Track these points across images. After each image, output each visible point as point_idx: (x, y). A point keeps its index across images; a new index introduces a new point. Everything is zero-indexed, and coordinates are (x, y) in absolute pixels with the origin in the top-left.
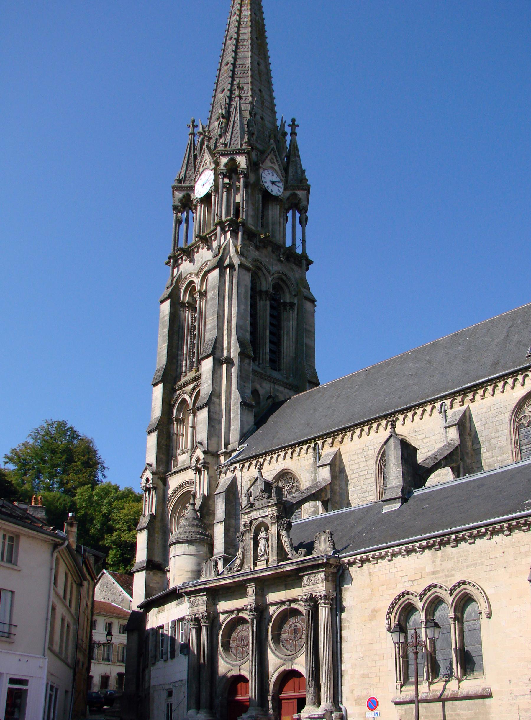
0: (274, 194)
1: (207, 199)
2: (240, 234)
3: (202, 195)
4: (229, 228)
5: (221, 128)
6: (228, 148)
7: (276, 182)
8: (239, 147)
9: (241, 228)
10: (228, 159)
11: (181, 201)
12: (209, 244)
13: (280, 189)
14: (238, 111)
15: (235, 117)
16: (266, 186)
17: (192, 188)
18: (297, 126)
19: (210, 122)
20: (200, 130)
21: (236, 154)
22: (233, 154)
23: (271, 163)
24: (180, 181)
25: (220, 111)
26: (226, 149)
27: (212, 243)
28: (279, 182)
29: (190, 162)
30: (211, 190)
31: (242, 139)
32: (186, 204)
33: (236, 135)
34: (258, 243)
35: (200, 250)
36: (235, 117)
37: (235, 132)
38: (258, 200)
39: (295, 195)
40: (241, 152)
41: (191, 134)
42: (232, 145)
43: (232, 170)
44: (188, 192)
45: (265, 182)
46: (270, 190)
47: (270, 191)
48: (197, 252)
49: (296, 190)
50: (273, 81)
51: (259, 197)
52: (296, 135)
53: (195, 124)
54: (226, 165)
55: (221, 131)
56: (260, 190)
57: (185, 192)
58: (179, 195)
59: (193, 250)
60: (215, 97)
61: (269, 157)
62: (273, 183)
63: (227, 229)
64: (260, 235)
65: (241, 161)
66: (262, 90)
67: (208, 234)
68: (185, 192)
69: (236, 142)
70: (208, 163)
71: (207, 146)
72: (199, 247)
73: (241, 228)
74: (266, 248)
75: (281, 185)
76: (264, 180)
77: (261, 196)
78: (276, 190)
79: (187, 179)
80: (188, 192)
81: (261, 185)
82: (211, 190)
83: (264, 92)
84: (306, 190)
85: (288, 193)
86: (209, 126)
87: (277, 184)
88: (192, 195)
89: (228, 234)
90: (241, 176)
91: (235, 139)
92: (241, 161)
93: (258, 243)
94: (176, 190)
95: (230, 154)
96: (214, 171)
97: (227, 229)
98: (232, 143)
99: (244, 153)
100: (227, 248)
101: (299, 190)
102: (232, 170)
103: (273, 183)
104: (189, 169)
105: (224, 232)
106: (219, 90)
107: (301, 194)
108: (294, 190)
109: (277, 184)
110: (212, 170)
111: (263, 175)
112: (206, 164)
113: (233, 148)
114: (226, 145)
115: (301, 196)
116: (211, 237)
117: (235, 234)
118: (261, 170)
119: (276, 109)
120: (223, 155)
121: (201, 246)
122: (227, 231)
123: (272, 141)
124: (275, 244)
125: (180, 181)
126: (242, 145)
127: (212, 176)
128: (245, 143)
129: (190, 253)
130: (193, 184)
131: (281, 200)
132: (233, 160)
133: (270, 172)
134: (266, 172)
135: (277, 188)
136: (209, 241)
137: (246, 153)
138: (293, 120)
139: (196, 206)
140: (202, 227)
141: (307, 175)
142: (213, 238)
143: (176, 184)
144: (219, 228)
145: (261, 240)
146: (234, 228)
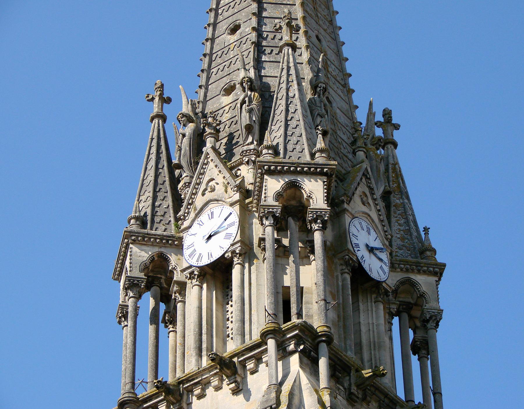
0: (374, 275)
1: (218, 274)
2: (323, 363)
3: (205, 261)
4: (297, 345)
5: (250, 111)
6: (280, 159)
7: (377, 249)
8: (308, 158)
9: (323, 348)
10: (282, 182)
11: (145, 268)
12: (239, 379)
13: (384, 266)
14: (294, 77)
15: (288, 90)
16: (359, 254)
17: (176, 243)
18: (397, 127)
19: (205, 96)
20: (186, 109)
21: (302, 173)
22: (295, 172)
23: (364, 204)
24: (142, 221)
25: (242, 74)
26: (277, 160)
27: (244, 378)
28: (381, 250)
29: (160, 181)
30: (233, 252)
31: (312, 143)
32: (158, 281)
33: (297, 132)
34: (354, 389)
35: (210, 391)
36: (288, 90)
37: (292, 124)
38: (344, 286)
39: (413, 284)
40: (314, 171)
41: (158, 116)
42: (289, 154)
43: (291, 211)
44: (163, 250)
45: (357, 245)
46: (366, 266)
47: (367, 268)
48: (201, 397)
49: (413, 271)
50: (339, 20)
51: (344, 280)
52: (395, 145)
53: (165, 96)
54: (278, 196)
55: (250, 118)
56: (347, 263)
57: (156, 250)
58: (140, 255)
59: (190, 391)
60: (213, 40)
61: (358, 192)
62: (371, 250)
63: (292, 347)
64: (358, 371)
65: (315, 191)
66: (321, 37)
67: (237, 354)
68: (156, 250)
69: (298, 147)
70: (219, 189)
71: (213, 148)
72: (209, 383)
73: (323, 348)
74: (368, 404)
75: (384, 256)
76: (354, 241)
77: (348, 277)
78: (377, 268)
79: (157, 219)
80: (163, 250)
81: (349, 250)
82: (233, 252)
83: (324, 43)
84: (435, 274)
85: (399, 276)
86: (205, 102)
87: (377, 252)
88: (173, 259)
89: (295, 359)
90: (315, 226)
91: (294, 139)
92: (315, 191)
93: (354, 389)
94: (134, 242)
95: (288, 172)
96: (237, 207)
97: (292, 347)
98: (290, 147)
99: (322, 174)
100: (296, 392)
101: (419, 272)
102: (291, 211)
103: (371, 250)
104: (160, 195)
105: (283, 354)
106: (223, 26)
107: (422, 280)
108: (407, 271)
109: (377, 252)
110: (232, 205)
111: (353, 230)
112: (213, 190)
113: (294, 159)
114: (275, 150)
115: (424, 288)
116: (243, 364)
117: (310, 362)
118: (347, 218)
119: (352, 83)
120: (271, 173)
121: (215, 382)
122: (292, 353)
123: (361, 155)
124: (386, 395)
125: (142, 221)
126: (313, 156)
127: (235, 218)
128: (321, 151)
129: (181, 395)
130: (172, 231)
131: (386, 292)
132: (294, 187)
133: (364, 224)
134: (356, 222)
135: (379, 263)
136: (240, 371)
137: (325, 174)
138: (387, 114)
139: (182, 286)
140: (204, 337)
141: (435, 240)
142: (250, 365)
143: (134, 227)
144: (271, 343)
145: (362, 383)
146: (308, 345)
